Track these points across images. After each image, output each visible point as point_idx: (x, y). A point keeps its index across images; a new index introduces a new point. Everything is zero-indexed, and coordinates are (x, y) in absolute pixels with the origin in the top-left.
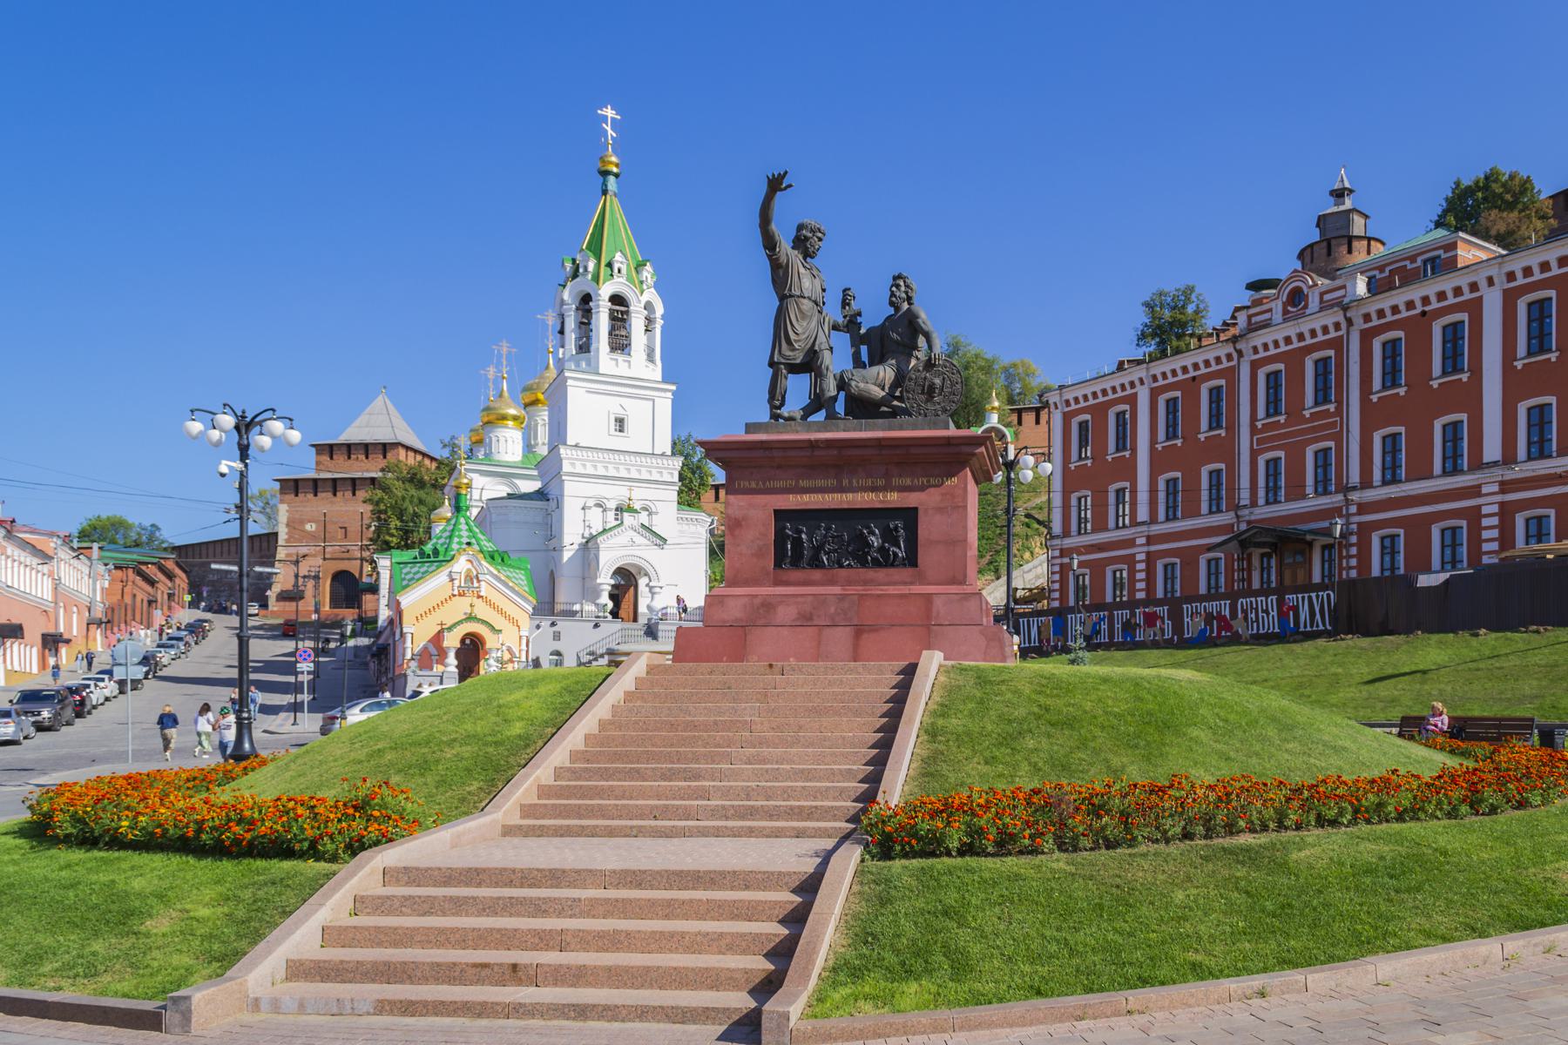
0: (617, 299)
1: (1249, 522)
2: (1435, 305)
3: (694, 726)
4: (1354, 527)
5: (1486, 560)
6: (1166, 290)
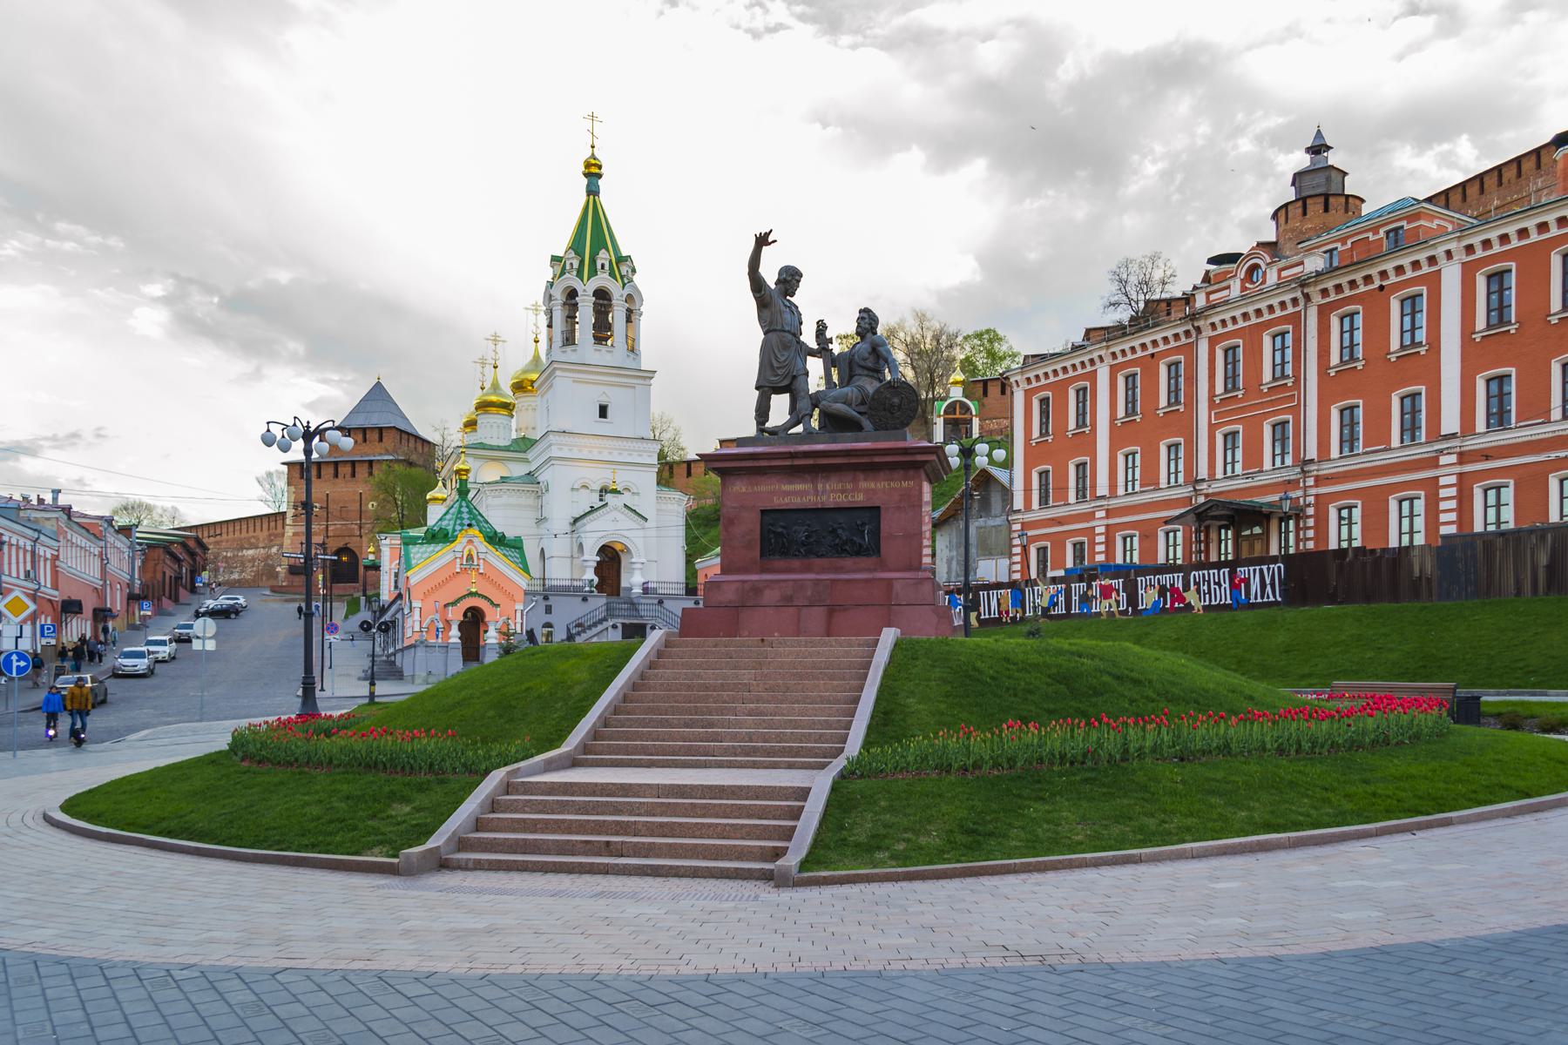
0: (602, 295)
1: (1207, 495)
2: (1393, 279)
3: (707, 688)
4: (1311, 499)
5: (1444, 530)
6: (1132, 256)
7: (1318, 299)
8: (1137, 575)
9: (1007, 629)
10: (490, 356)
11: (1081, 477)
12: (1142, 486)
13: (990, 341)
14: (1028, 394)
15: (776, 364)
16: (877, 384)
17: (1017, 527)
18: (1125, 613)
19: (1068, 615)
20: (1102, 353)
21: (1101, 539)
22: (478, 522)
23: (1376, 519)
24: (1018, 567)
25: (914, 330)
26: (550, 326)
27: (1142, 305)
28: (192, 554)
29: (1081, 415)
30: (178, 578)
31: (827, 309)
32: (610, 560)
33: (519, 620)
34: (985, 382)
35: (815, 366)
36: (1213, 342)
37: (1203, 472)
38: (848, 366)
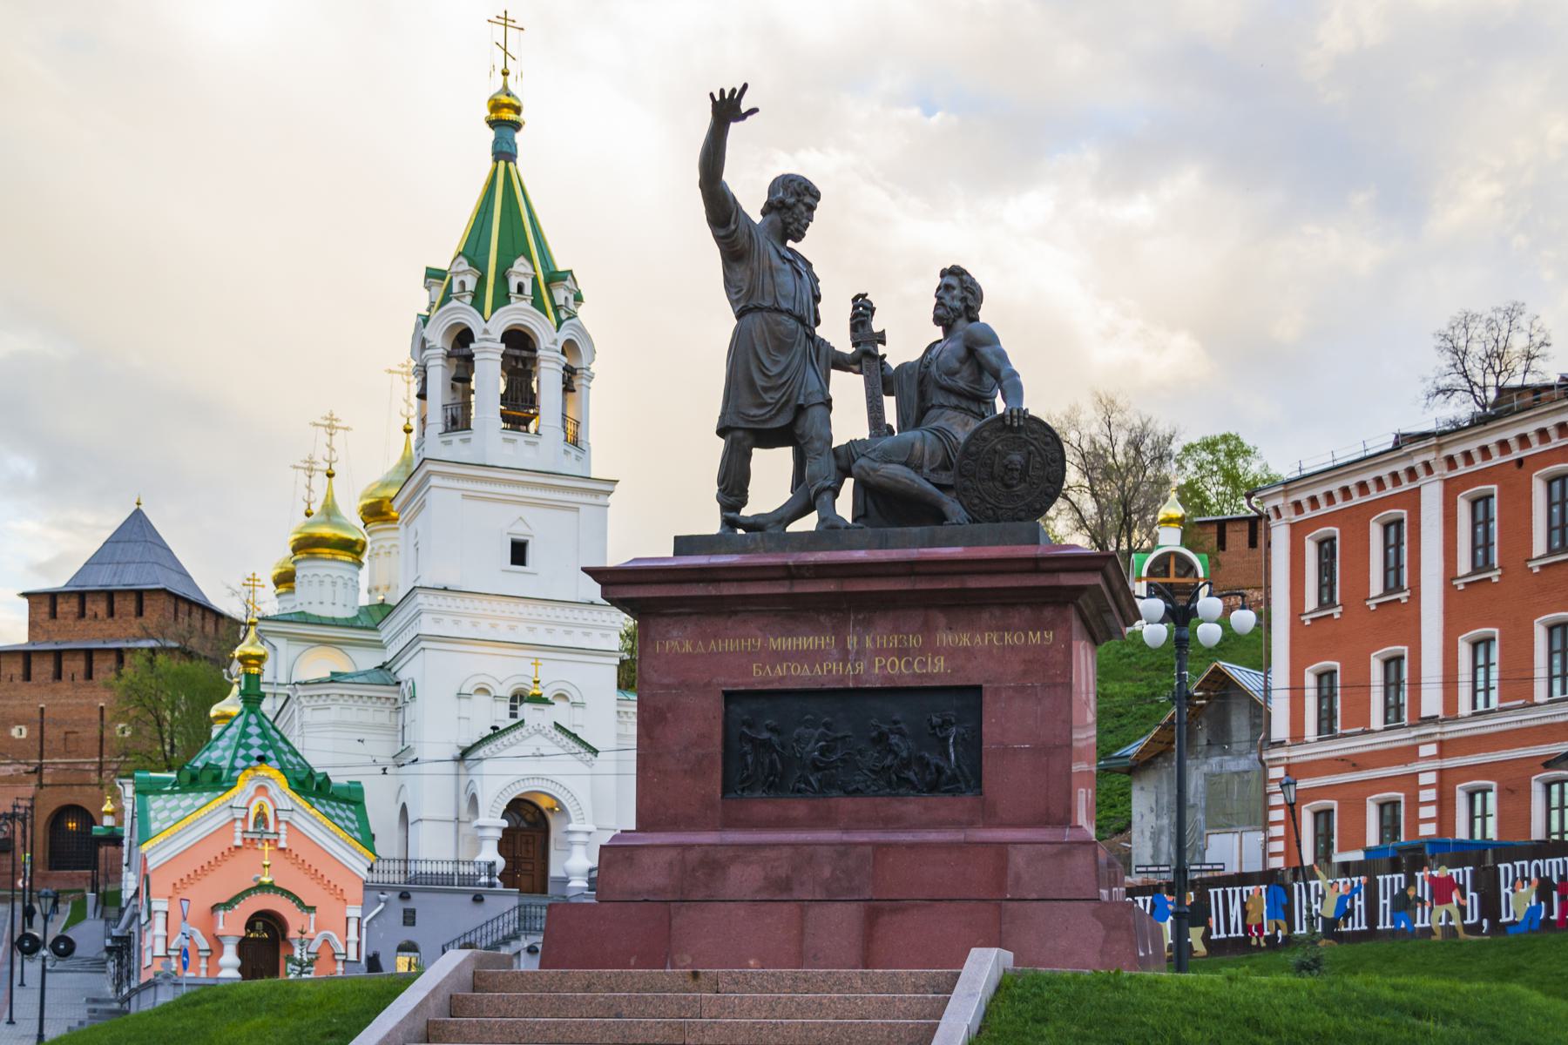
0: (519, 342)
8: (1499, 858)
9: (1259, 958)
10: (321, 453)
11: (1392, 684)
12: (1501, 700)
13: (1231, 455)
15: (760, 381)
16: (974, 424)
17: (1277, 773)
18: (1475, 929)
19: (1372, 933)
20: (1430, 457)
21: (1429, 795)
22: (278, 752)
24: (1279, 846)
25: (1094, 429)
26: (422, 396)
27: (1492, 394)
29: (1392, 569)
31: (875, 265)
32: (529, 825)
33: (353, 936)
34: (1222, 525)
35: (847, 390)
38: (918, 388)
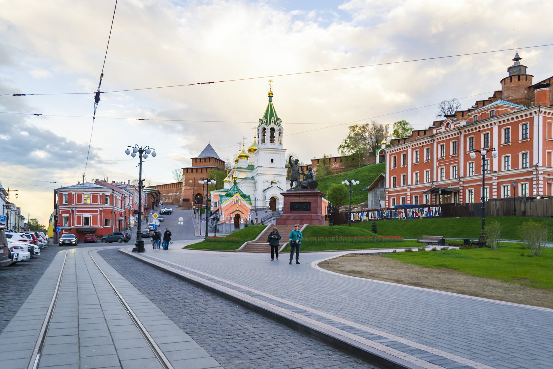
0: (272, 129)
2: (482, 129)
7: (463, 133)
11: (404, 180)
13: (404, 124)
14: (390, 155)
18: (404, 218)
21: (409, 197)
23: (514, 189)
28: (157, 196)
30: (154, 203)
32: (273, 201)
36: (438, 143)
37: (435, 179)
